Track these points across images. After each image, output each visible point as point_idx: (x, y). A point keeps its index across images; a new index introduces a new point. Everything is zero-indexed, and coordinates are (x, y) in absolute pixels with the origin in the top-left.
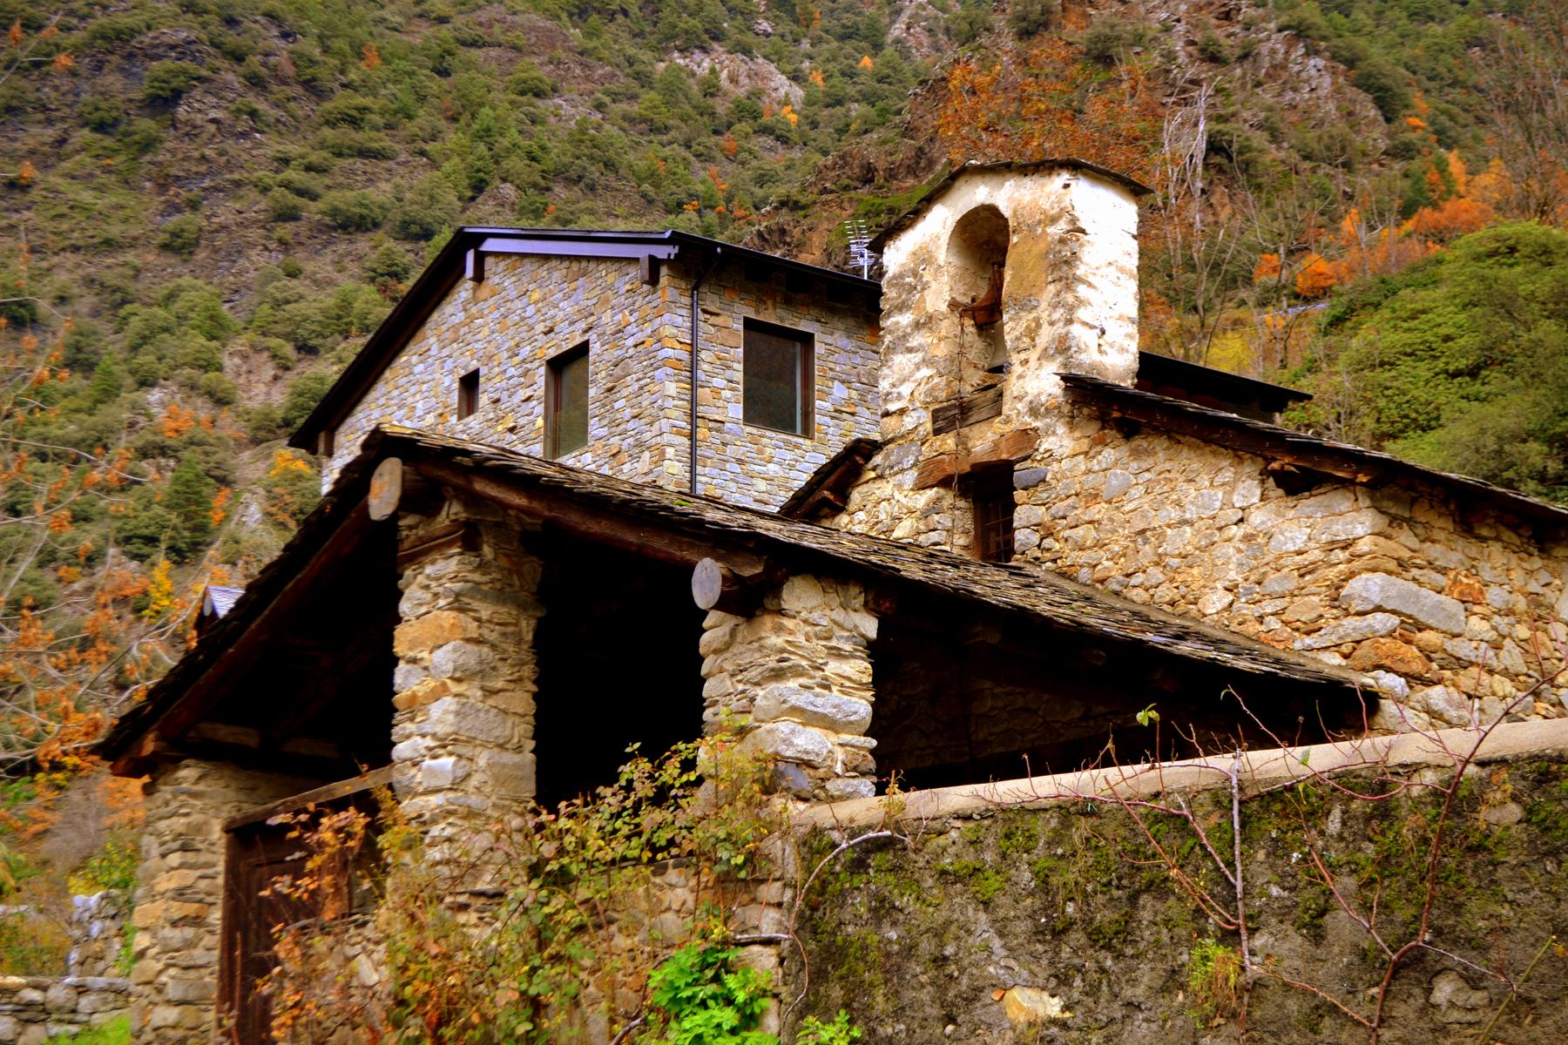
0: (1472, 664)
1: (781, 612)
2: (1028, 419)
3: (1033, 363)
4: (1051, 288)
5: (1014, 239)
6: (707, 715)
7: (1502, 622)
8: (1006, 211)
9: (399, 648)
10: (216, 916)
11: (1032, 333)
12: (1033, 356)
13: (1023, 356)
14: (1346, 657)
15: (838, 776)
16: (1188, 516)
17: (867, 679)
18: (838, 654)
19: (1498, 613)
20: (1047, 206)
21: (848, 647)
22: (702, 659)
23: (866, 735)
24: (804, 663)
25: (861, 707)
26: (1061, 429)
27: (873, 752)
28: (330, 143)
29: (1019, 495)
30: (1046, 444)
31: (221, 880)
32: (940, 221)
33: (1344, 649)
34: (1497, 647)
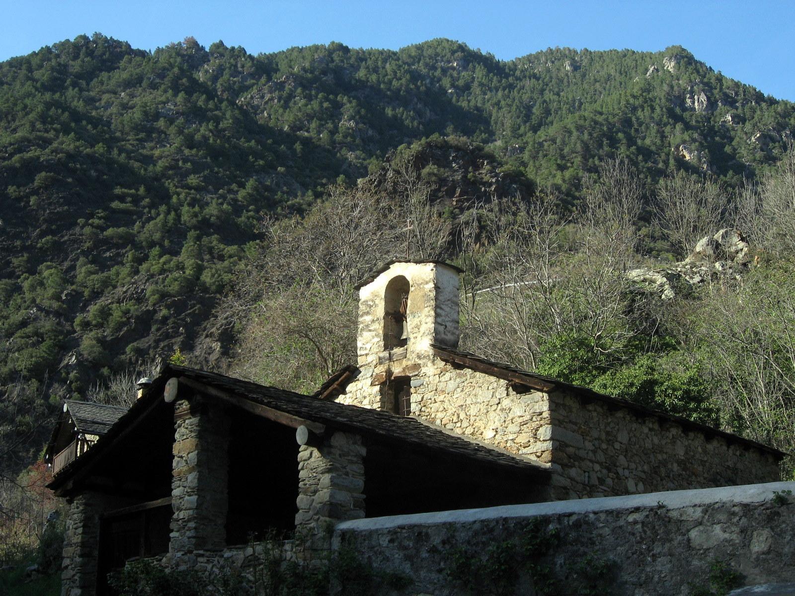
0: (585, 459)
1: (331, 446)
2: (416, 360)
3: (419, 337)
4: (426, 309)
5: (412, 289)
6: (301, 484)
7: (596, 443)
8: (409, 278)
9: (175, 452)
10: (96, 553)
11: (418, 327)
12: (419, 336)
13: (415, 335)
14: (538, 457)
15: (351, 510)
16: (479, 400)
17: (363, 472)
18: (352, 462)
19: (596, 439)
20: (425, 277)
21: (355, 459)
22: (298, 463)
23: (362, 493)
24: (339, 466)
25: (360, 482)
26: (430, 364)
27: (364, 500)
28: (65, 150)
29: (412, 390)
30: (424, 370)
31: (98, 539)
32: (383, 280)
33: (538, 454)
34: (594, 452)
